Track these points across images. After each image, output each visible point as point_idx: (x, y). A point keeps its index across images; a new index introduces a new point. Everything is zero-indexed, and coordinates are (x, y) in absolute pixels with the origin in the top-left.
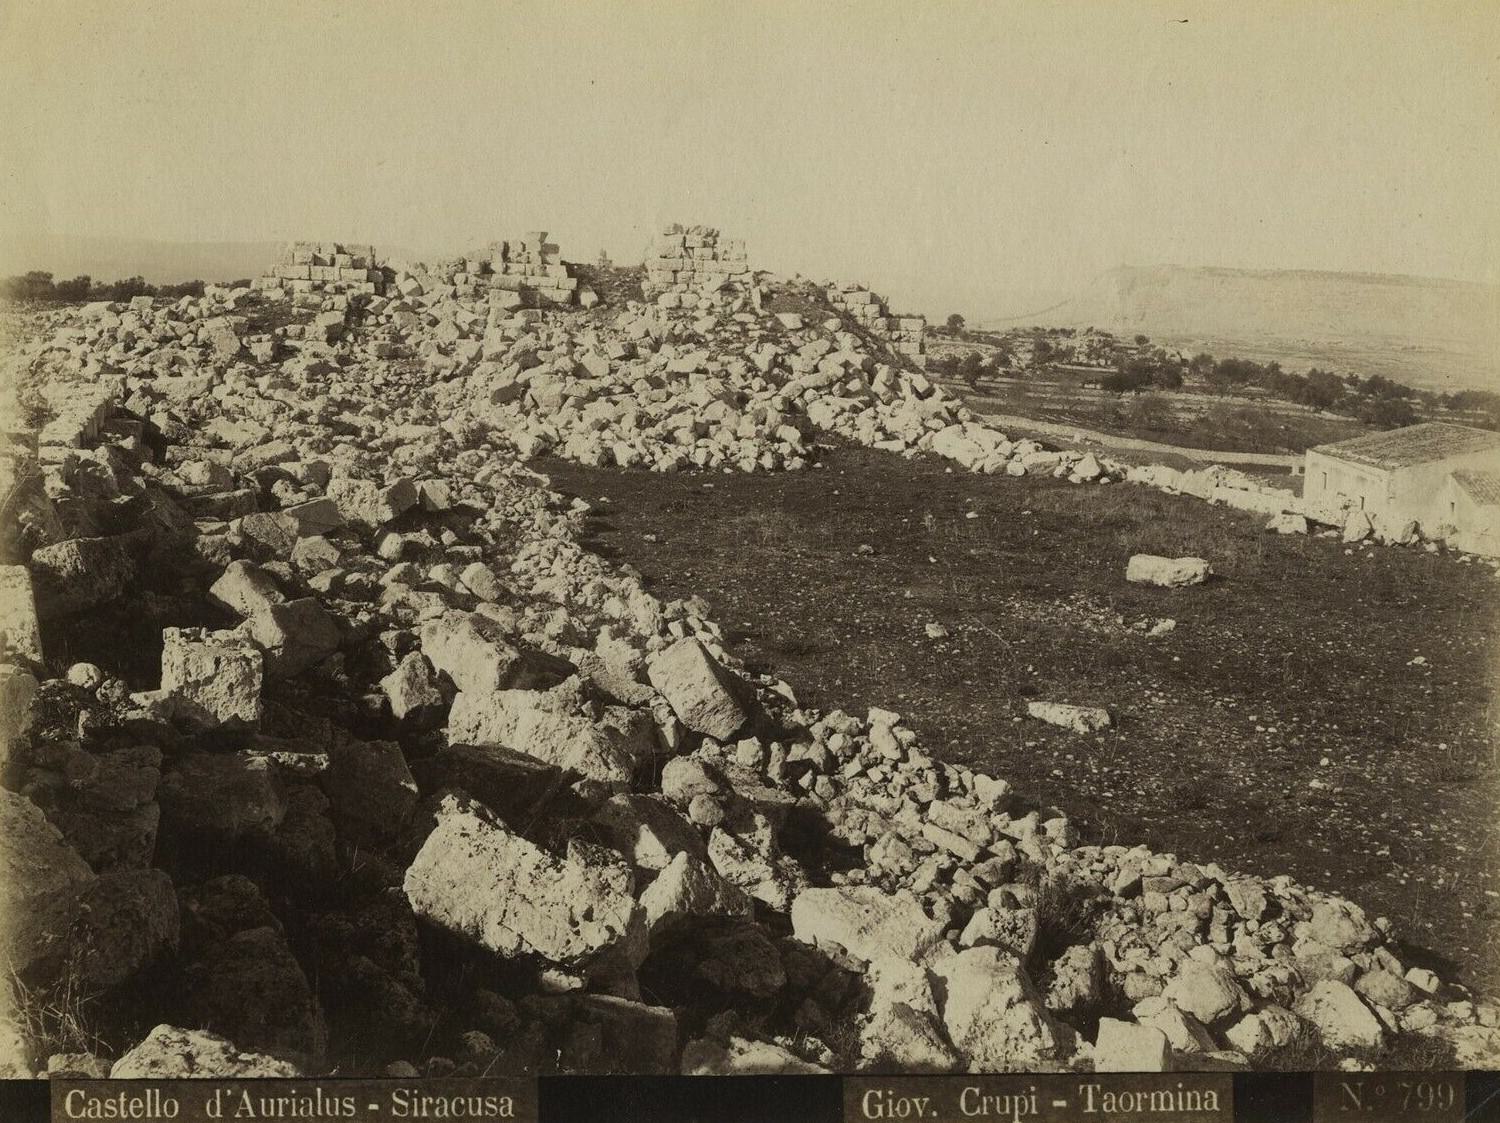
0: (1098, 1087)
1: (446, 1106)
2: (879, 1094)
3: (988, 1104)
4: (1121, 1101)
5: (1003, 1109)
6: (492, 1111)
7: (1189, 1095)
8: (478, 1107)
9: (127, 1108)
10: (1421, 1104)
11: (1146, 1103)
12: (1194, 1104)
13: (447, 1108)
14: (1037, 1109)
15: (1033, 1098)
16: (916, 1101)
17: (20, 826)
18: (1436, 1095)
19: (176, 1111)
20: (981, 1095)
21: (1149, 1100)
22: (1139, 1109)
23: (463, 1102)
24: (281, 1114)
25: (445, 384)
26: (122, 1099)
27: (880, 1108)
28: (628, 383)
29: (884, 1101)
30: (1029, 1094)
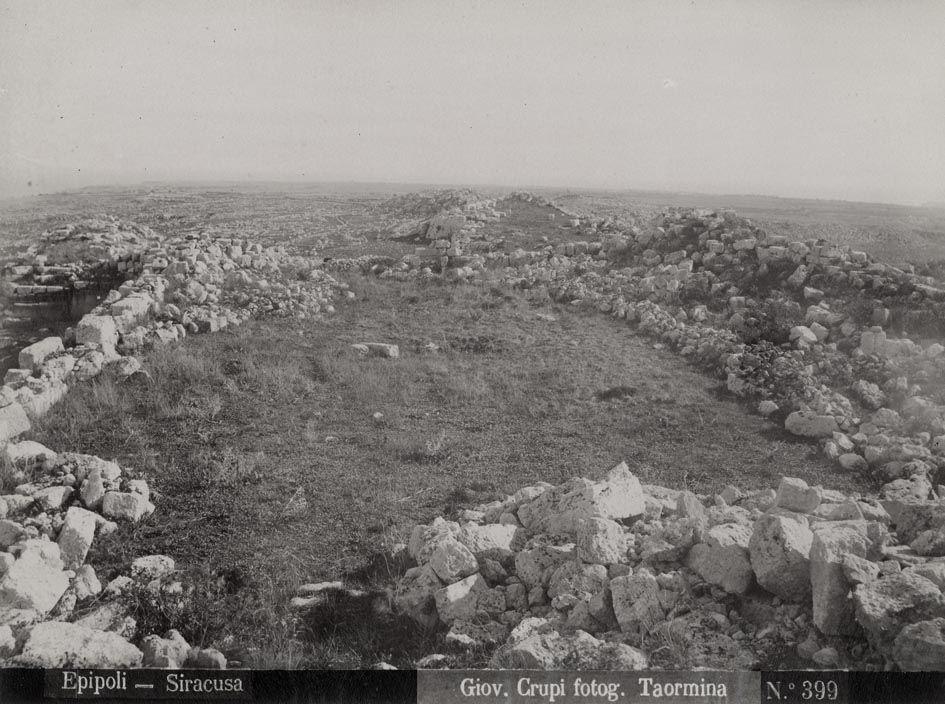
0: (651, 680)
1: (200, 684)
2: (472, 681)
3: (679, 689)
5: (543, 692)
9: (596, 689)
10: (804, 694)
11: (681, 691)
12: (711, 691)
15: (124, 679)
16: (494, 685)
18: (826, 690)
24: (187, 690)
30: (559, 683)
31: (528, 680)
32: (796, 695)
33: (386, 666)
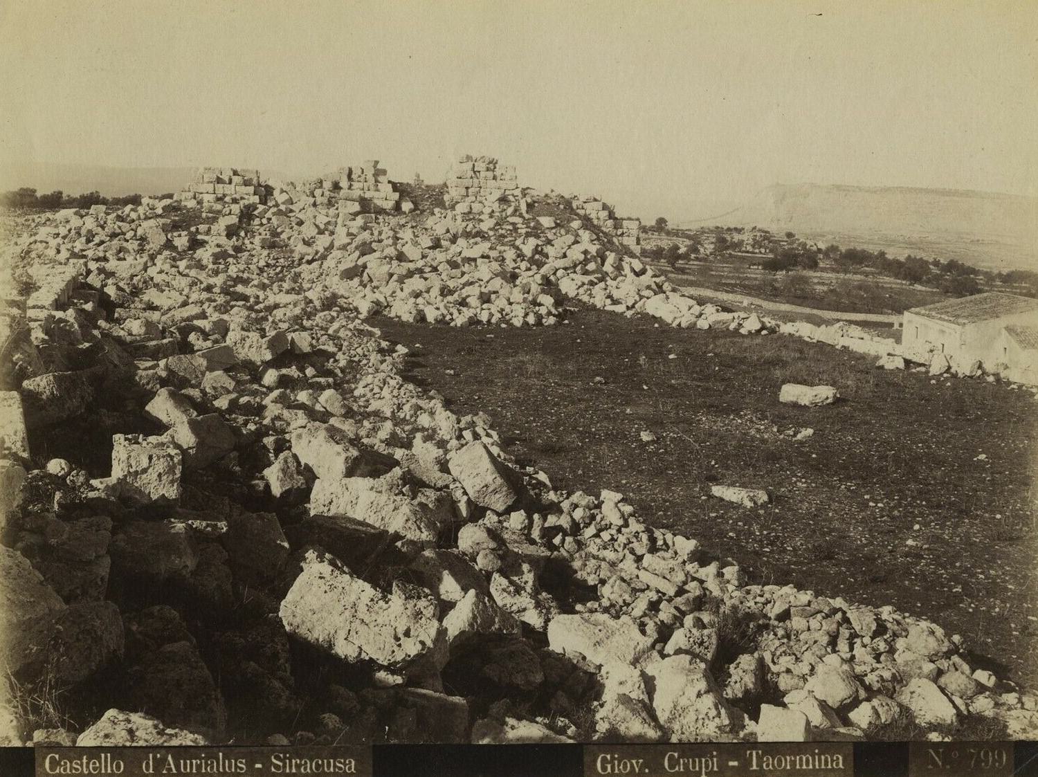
0: (760, 752)
1: (309, 765)
2: (609, 757)
4: (776, 762)
5: (694, 767)
6: (340, 769)
7: (823, 757)
8: (331, 766)
9: (88, 767)
11: (793, 763)
12: (826, 764)
13: (309, 767)
14: (717, 767)
15: (715, 759)
16: (634, 762)
17: (14, 571)
18: (994, 758)
19: (122, 769)
20: (679, 758)
21: (795, 761)
22: (788, 767)
23: (320, 762)
24: (194, 771)
25: (308, 266)
26: (85, 761)
27: (609, 766)
28: (435, 265)
29: (612, 762)
30: (712, 757)
31: (676, 755)
32: (656, 767)
33: (486, 741)
